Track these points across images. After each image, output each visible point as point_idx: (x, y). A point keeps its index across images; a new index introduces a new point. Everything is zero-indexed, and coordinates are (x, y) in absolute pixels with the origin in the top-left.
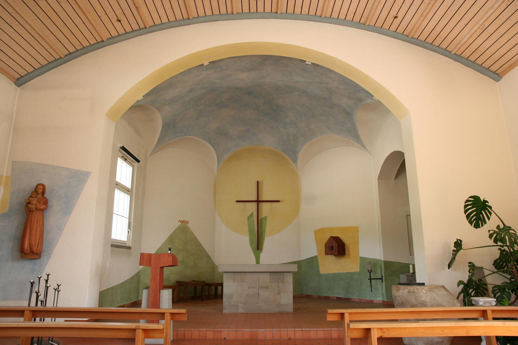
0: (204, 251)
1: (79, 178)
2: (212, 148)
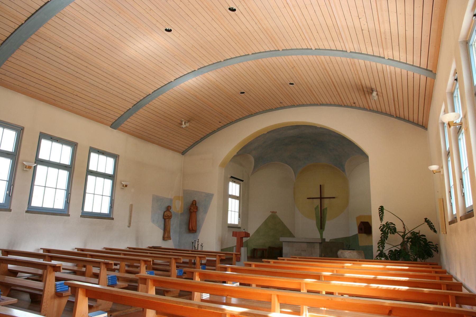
0: (288, 230)
1: (209, 196)
2: (289, 167)
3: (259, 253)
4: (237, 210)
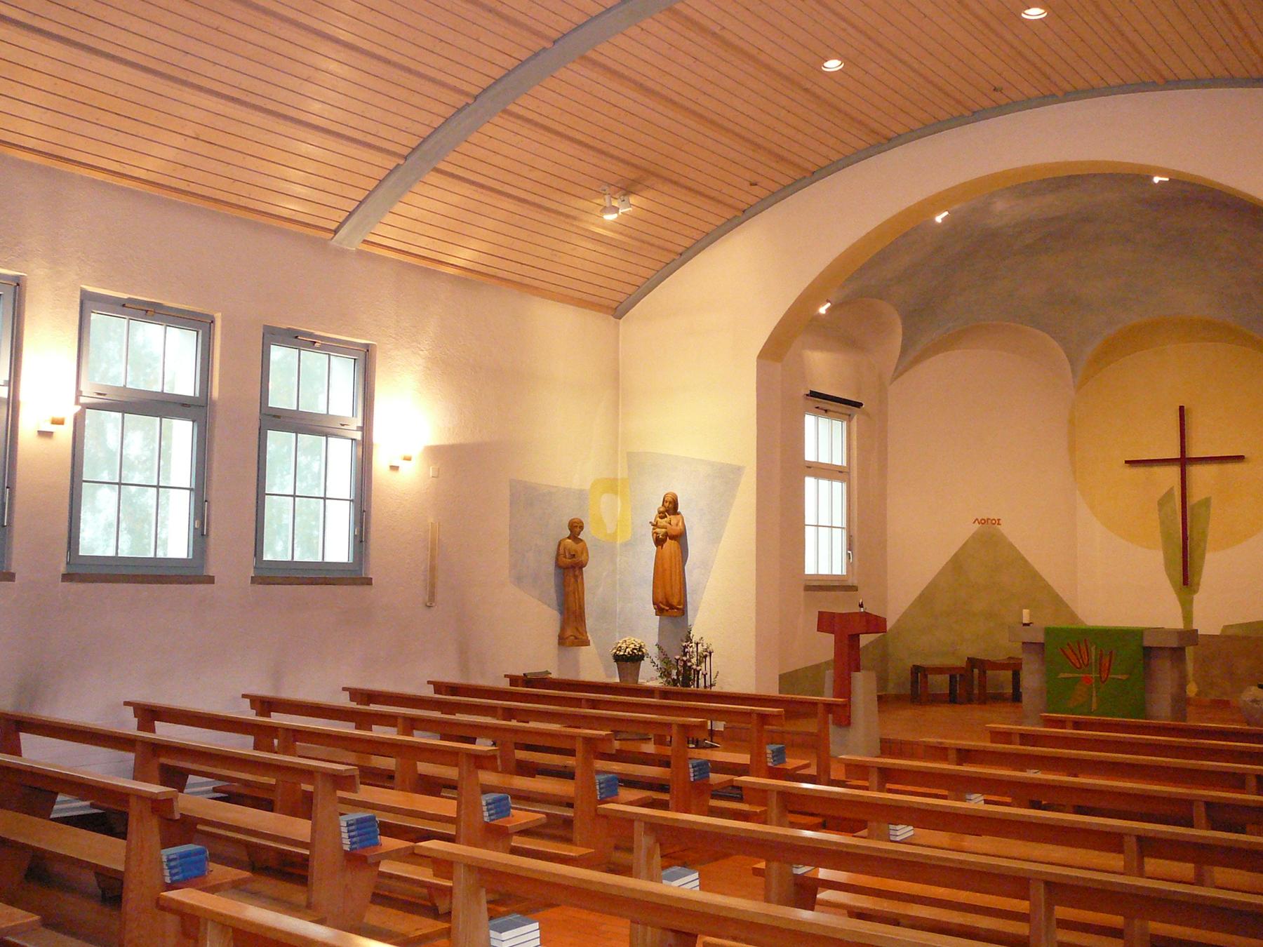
0: (1047, 587)
2: (1055, 343)
3: (940, 683)
4: (839, 519)
